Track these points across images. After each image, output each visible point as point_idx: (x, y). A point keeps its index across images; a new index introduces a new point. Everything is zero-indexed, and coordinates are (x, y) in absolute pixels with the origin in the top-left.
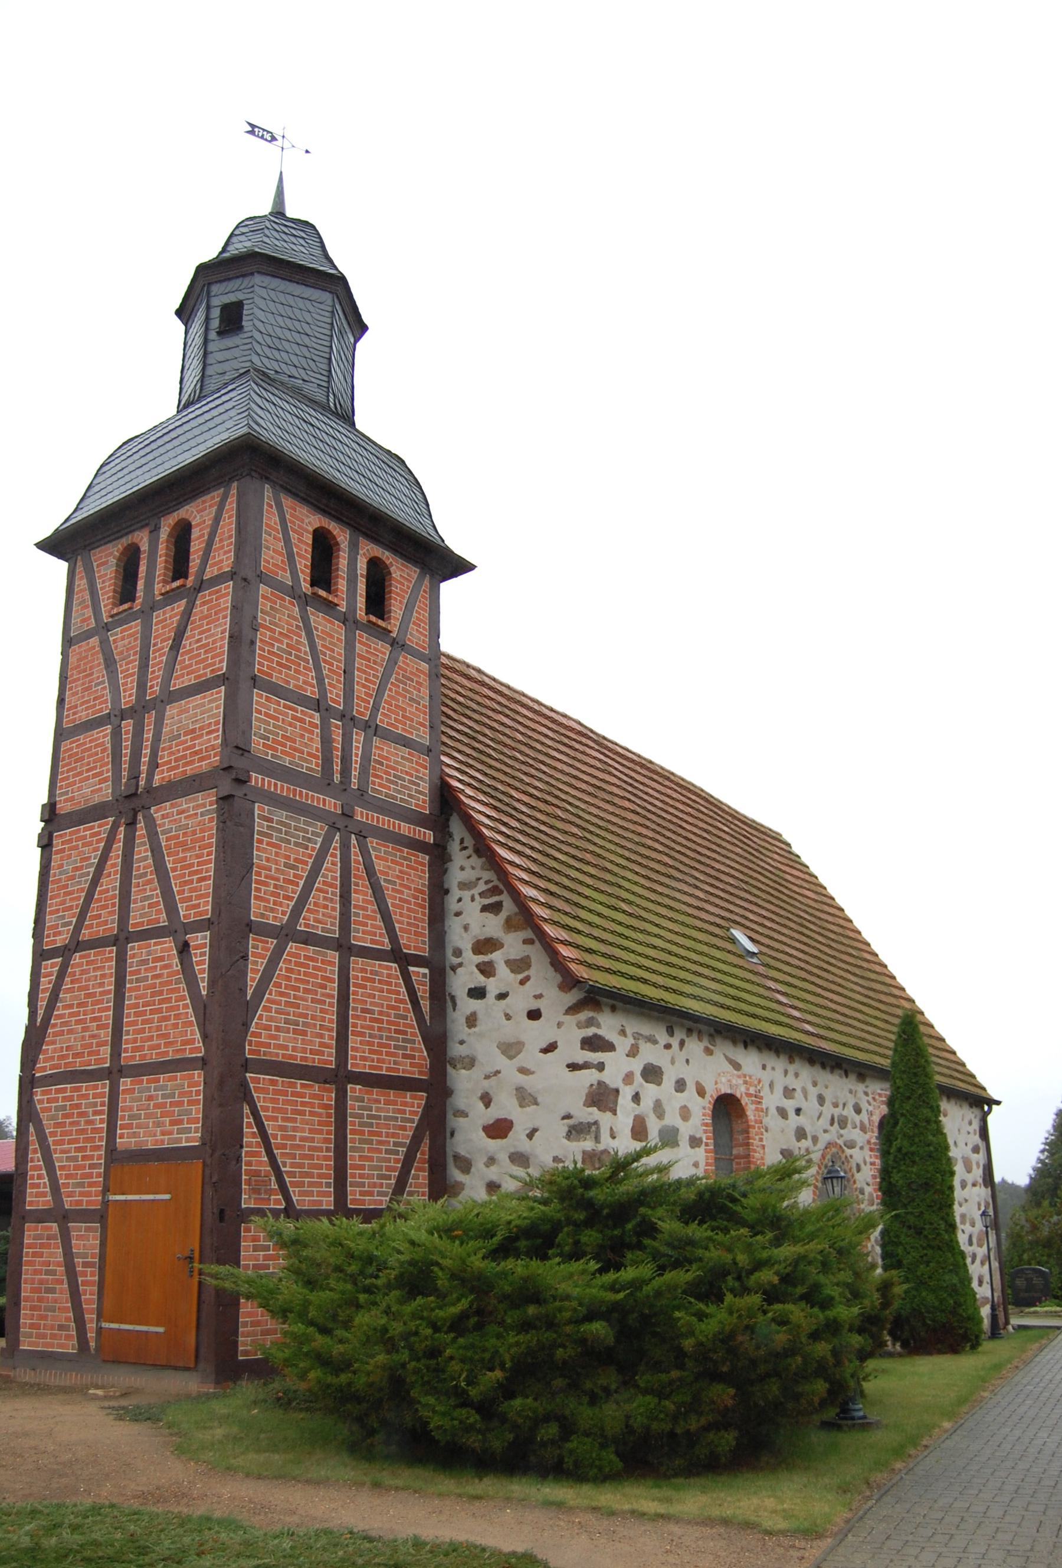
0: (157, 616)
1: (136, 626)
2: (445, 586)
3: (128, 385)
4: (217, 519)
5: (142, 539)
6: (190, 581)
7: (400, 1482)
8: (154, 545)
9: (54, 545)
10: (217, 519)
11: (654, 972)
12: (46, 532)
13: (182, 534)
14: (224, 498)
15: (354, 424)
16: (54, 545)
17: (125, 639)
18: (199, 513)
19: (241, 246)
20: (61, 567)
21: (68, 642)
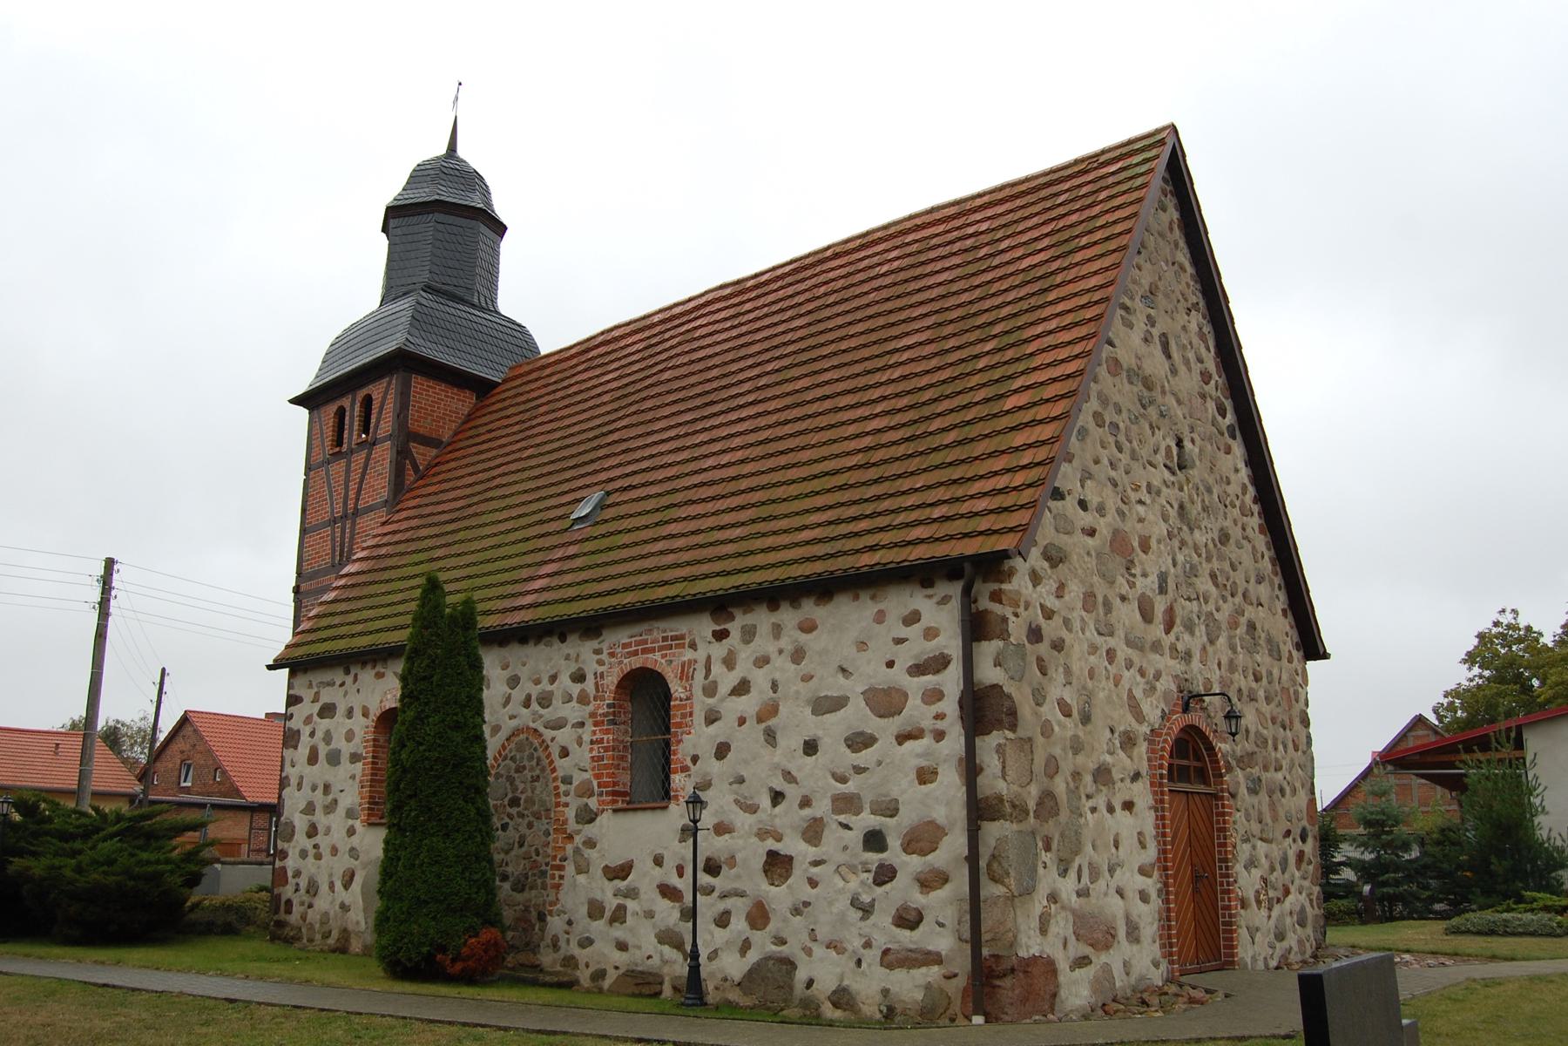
0: (355, 457)
1: (343, 462)
2: (549, 341)
3: (345, 282)
4: (386, 393)
5: (346, 402)
6: (345, 447)
7: (332, 977)
8: (352, 405)
9: (297, 401)
10: (386, 393)
11: (561, 448)
12: (302, 388)
13: (368, 401)
14: (389, 383)
15: (498, 313)
16: (297, 401)
17: (338, 468)
18: (376, 390)
19: (423, 195)
20: (303, 413)
21: (309, 468)
